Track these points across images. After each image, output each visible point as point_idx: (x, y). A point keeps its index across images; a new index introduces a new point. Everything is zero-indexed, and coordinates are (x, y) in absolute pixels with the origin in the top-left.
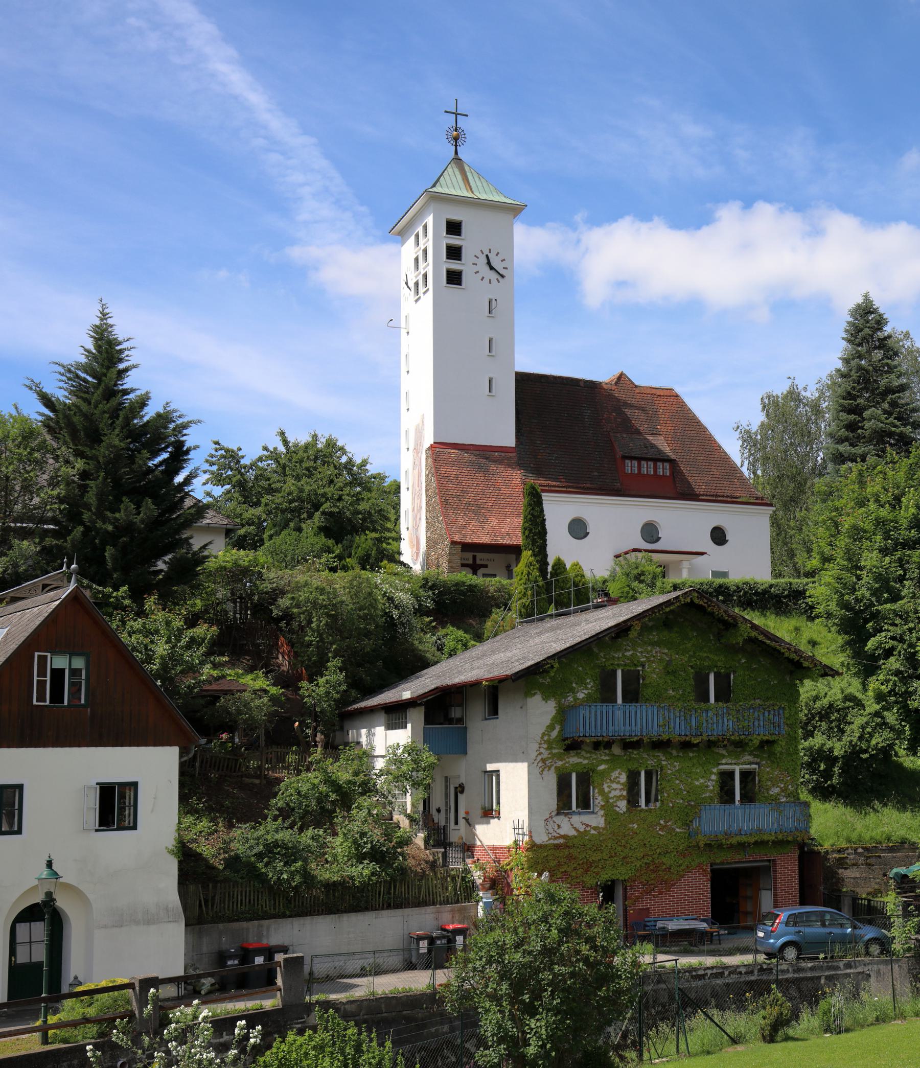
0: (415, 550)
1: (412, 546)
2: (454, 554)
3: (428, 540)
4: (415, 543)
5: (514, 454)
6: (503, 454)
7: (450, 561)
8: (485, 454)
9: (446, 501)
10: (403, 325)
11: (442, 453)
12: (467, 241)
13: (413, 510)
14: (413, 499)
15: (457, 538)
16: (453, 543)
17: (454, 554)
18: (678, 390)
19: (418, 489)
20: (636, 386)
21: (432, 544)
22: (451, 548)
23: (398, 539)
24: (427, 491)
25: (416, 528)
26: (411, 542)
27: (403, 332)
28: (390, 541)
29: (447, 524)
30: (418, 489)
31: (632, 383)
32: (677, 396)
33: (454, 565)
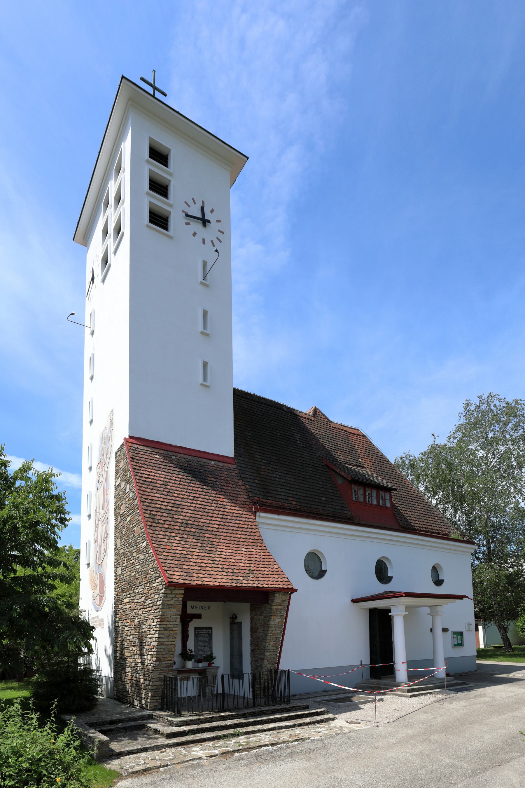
0: (97, 591)
1: (94, 587)
2: (170, 606)
3: (118, 579)
4: (98, 583)
5: (234, 466)
6: (221, 464)
7: (163, 619)
8: (195, 465)
9: (153, 517)
10: (87, 323)
11: (141, 450)
12: (176, 175)
13: (96, 541)
14: (97, 527)
15: (178, 577)
16: (171, 585)
17: (170, 606)
18: (364, 431)
19: (102, 512)
20: (330, 422)
21: (124, 587)
22: (166, 595)
23: (71, 579)
24: (117, 508)
25: (100, 563)
26: (93, 581)
27: (88, 331)
28: (57, 583)
29: (157, 553)
30: (102, 512)
31: (326, 418)
32: (364, 436)
33: (170, 625)
